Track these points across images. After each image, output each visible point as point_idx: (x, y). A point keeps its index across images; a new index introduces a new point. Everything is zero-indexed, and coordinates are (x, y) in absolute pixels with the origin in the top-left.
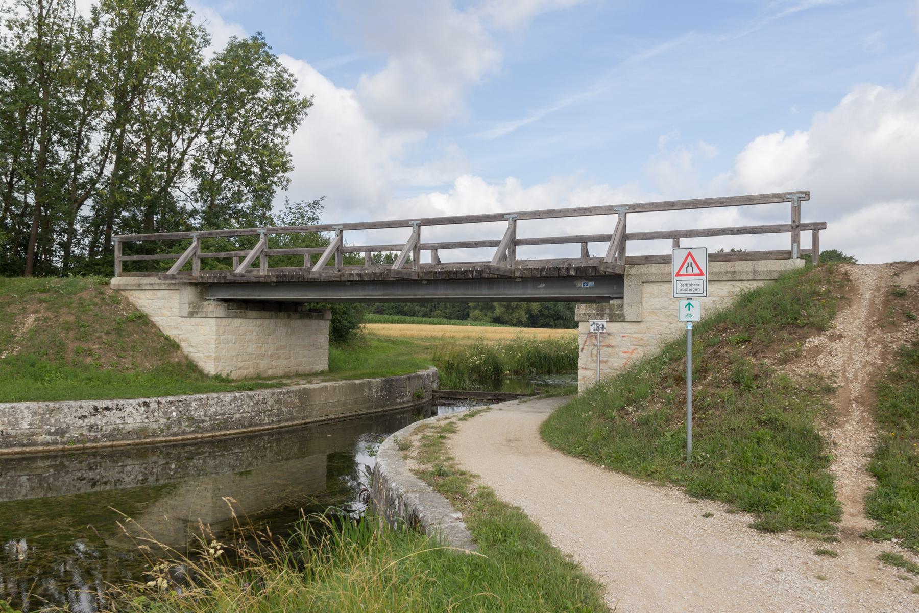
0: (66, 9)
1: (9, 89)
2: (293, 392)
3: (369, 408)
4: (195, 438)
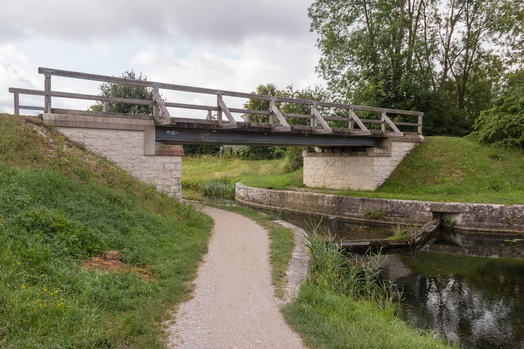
0: (486, 40)
1: (414, 67)
2: (277, 193)
3: (320, 212)
4: (490, 232)
